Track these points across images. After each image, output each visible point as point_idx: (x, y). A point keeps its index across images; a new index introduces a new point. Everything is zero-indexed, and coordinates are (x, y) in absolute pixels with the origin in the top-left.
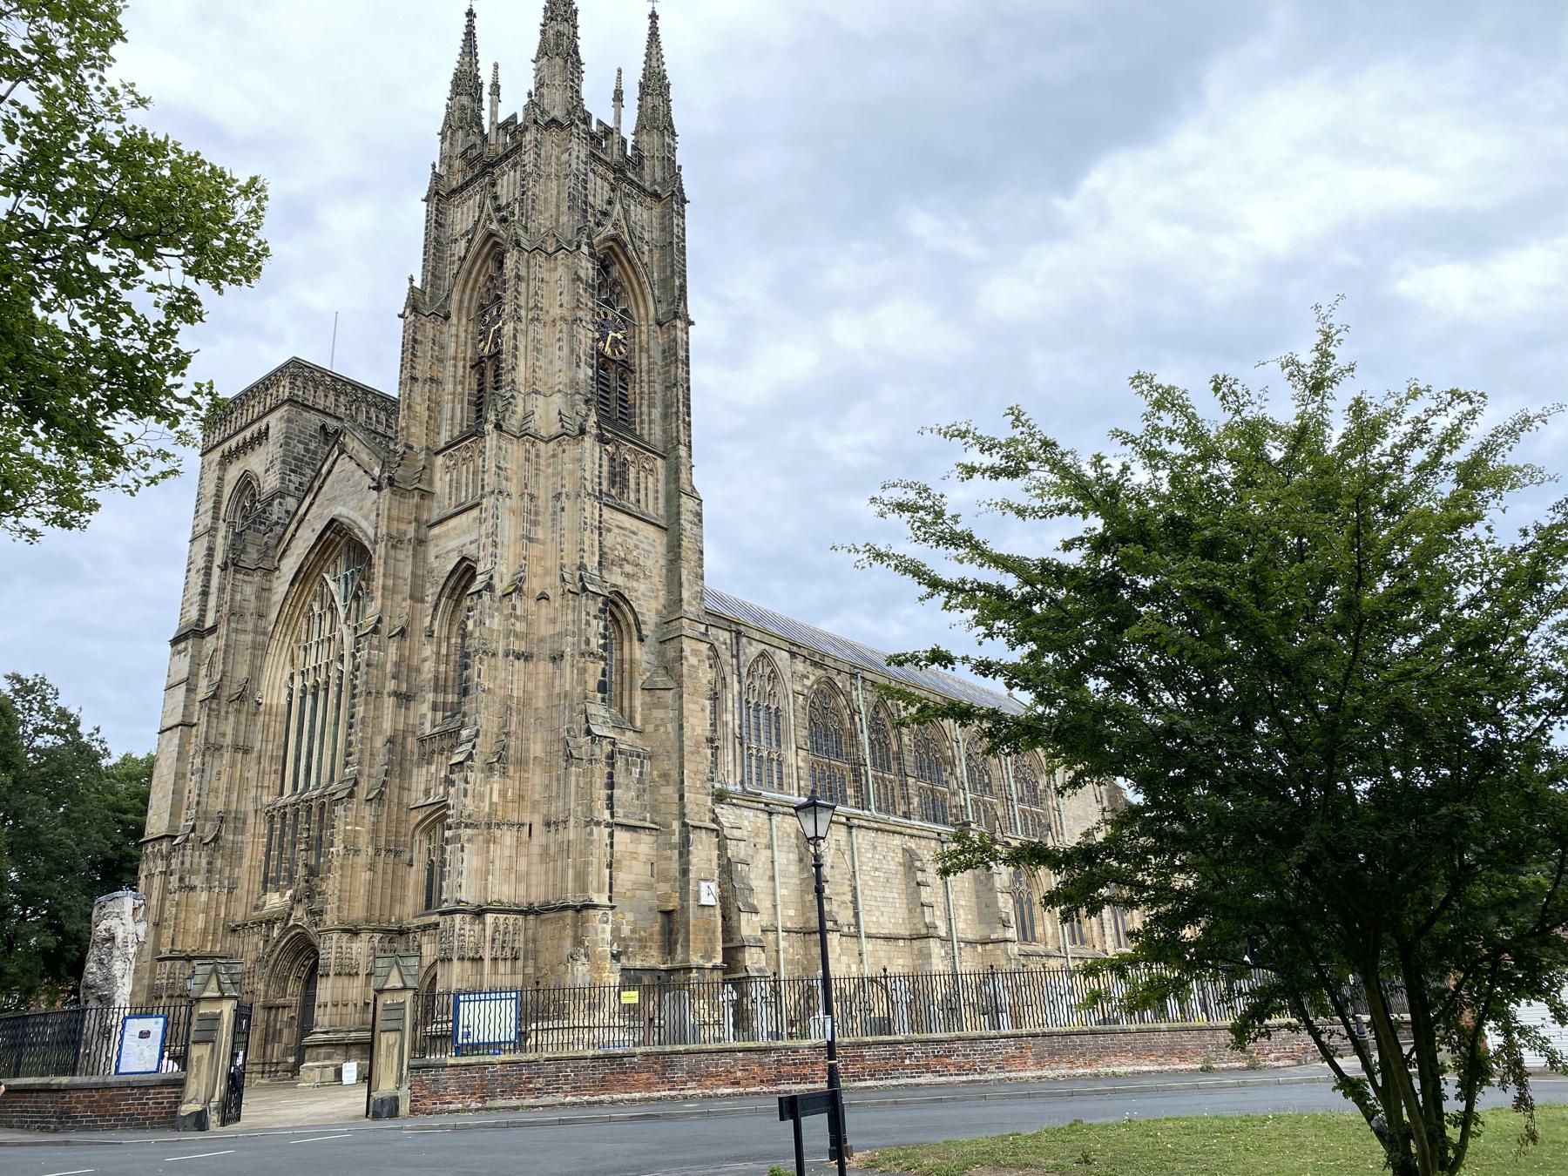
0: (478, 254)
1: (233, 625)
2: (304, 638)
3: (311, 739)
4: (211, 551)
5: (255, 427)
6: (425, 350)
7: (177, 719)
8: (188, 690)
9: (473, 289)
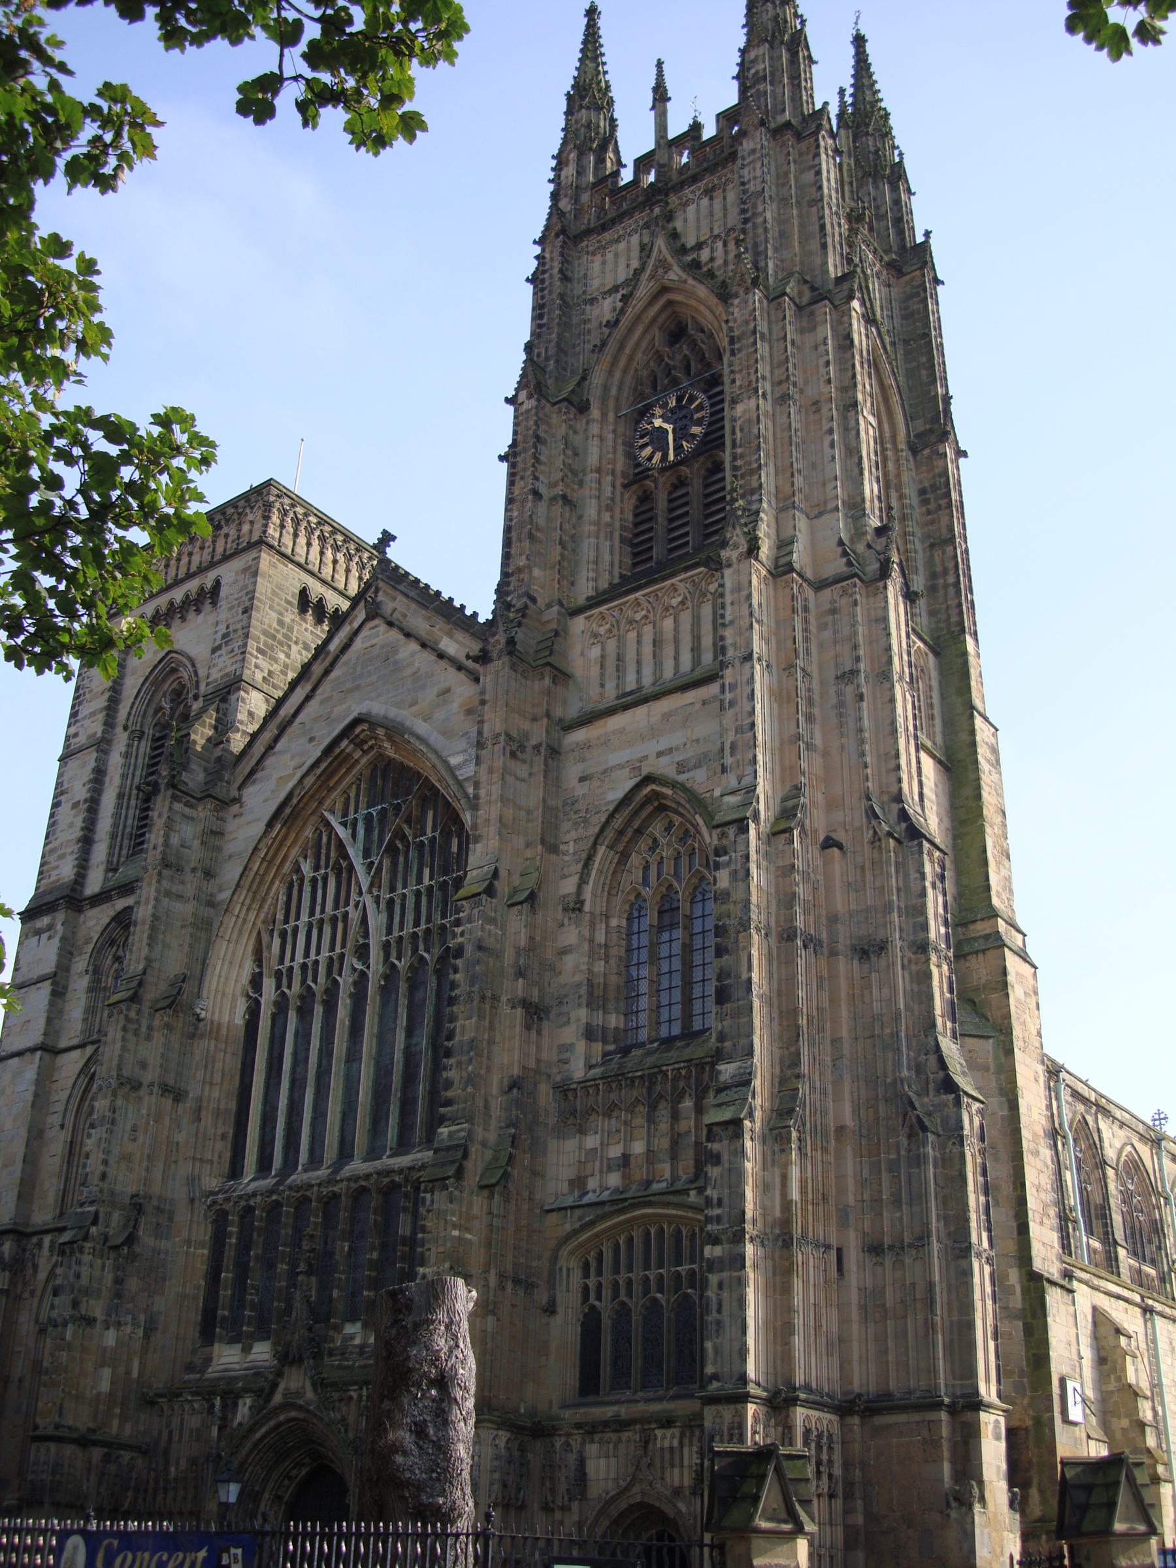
0: (638, 318)
1: (165, 884)
2: (280, 916)
3: (297, 1085)
4: (99, 774)
5: (193, 585)
6: (554, 457)
7: (34, 1037)
8: (54, 993)
9: (625, 371)
